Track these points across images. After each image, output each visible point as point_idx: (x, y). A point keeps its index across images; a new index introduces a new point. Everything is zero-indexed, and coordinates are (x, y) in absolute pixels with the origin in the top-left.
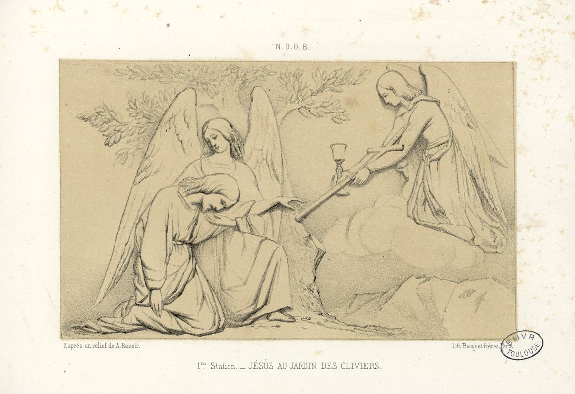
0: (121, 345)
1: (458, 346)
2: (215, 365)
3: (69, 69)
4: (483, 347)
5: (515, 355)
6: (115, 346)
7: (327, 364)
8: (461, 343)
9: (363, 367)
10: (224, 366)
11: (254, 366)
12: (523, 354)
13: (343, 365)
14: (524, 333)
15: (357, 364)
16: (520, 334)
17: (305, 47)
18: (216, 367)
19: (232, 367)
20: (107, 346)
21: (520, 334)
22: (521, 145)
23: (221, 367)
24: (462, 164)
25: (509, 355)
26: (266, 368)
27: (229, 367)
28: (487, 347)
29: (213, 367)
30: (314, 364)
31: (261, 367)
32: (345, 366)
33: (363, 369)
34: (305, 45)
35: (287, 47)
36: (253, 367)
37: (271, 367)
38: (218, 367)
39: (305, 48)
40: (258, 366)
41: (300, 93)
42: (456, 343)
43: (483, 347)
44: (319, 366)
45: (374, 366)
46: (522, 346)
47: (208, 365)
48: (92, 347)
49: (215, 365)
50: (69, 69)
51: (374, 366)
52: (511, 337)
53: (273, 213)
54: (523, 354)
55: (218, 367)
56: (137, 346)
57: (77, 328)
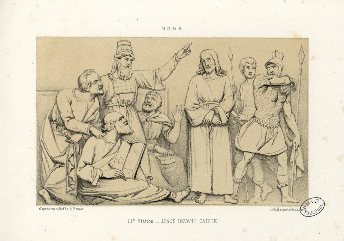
0: (72, 209)
1: (274, 210)
3: (50, 49)
4: (289, 210)
6: (69, 209)
7: (181, 220)
8: (276, 208)
9: (214, 222)
10: (146, 221)
11: (164, 221)
12: (314, 212)
13: (150, 221)
14: (312, 200)
15: (188, 222)
16: (309, 201)
17: (180, 29)
18: (141, 221)
19: (151, 222)
20: (64, 209)
21: (309, 201)
23: (144, 222)
25: (306, 215)
26: (171, 222)
27: (150, 222)
29: (139, 222)
30: (192, 220)
31: (168, 222)
32: (181, 221)
33: (212, 223)
35: (174, 29)
36: (163, 222)
37: (174, 222)
38: (142, 221)
39: (180, 29)
40: (166, 221)
41: (232, 69)
42: (273, 207)
43: (289, 210)
44: (177, 221)
45: (214, 221)
46: (312, 207)
47: (136, 221)
48: (55, 209)
50: (50, 49)
51: (214, 221)
52: (306, 203)
54: (314, 212)
55: (142, 221)
57: (48, 197)
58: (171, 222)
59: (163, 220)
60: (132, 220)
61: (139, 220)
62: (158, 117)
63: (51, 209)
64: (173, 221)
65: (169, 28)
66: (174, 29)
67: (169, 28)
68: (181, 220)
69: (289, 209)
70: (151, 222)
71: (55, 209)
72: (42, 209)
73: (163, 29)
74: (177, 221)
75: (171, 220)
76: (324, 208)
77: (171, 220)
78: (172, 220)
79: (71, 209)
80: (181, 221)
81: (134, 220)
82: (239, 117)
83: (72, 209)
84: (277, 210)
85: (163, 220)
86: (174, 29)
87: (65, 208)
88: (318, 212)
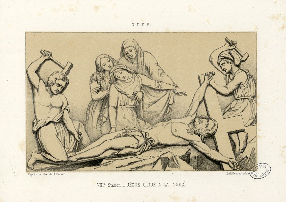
0: (56, 174)
1: (230, 174)
2: (110, 184)
4: (243, 174)
5: (257, 176)
6: (53, 174)
11: (130, 185)
12: (261, 175)
14: (260, 165)
17: (148, 25)
18: (110, 185)
19: (119, 185)
22: (86, 140)
24: (88, 121)
28: (245, 174)
29: (109, 186)
32: (110, 185)
34: (148, 24)
35: (138, 25)
36: (129, 186)
37: (139, 186)
38: (112, 185)
39: (148, 25)
40: (132, 185)
46: (260, 171)
48: (41, 175)
49: (110, 184)
53: (176, 95)
54: (261, 175)
55: (112, 185)
56: (64, 174)
57: (42, 161)
58: (136, 186)
59: (129, 184)
60: (104, 184)
61: (109, 184)
62: (96, 92)
63: (37, 174)
64: (154, 185)
65: (143, 24)
66: (138, 25)
67: (143, 24)
68: (180, 184)
69: (243, 173)
70: (119, 185)
71: (41, 175)
72: (31, 175)
73: (133, 25)
74: (141, 185)
75: (136, 184)
76: (270, 172)
77: (136, 184)
78: (137, 184)
79: (54, 175)
80: (110, 185)
81: (105, 184)
82: (137, 97)
83: (56, 174)
84: (232, 174)
85: (129, 184)
86: (138, 25)
87: (49, 174)
88: (265, 175)
